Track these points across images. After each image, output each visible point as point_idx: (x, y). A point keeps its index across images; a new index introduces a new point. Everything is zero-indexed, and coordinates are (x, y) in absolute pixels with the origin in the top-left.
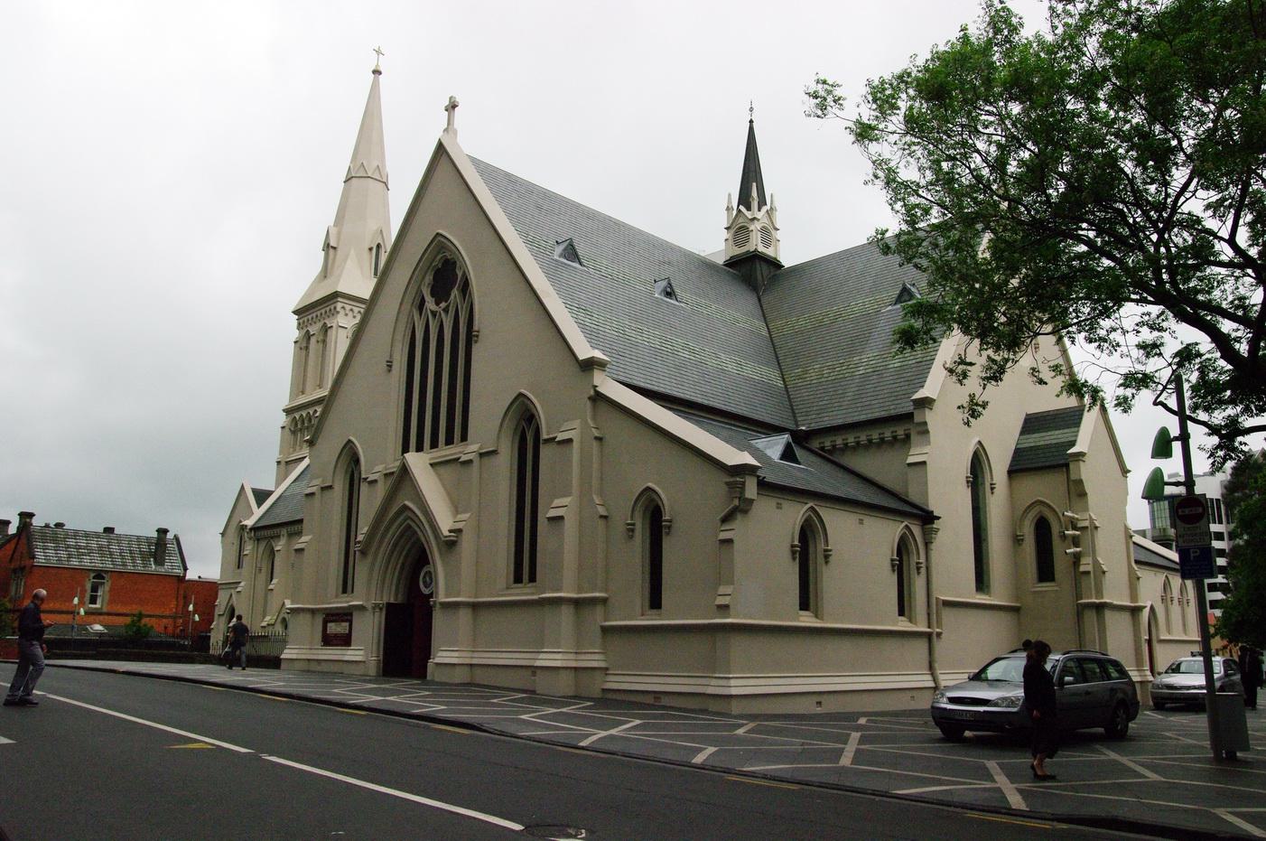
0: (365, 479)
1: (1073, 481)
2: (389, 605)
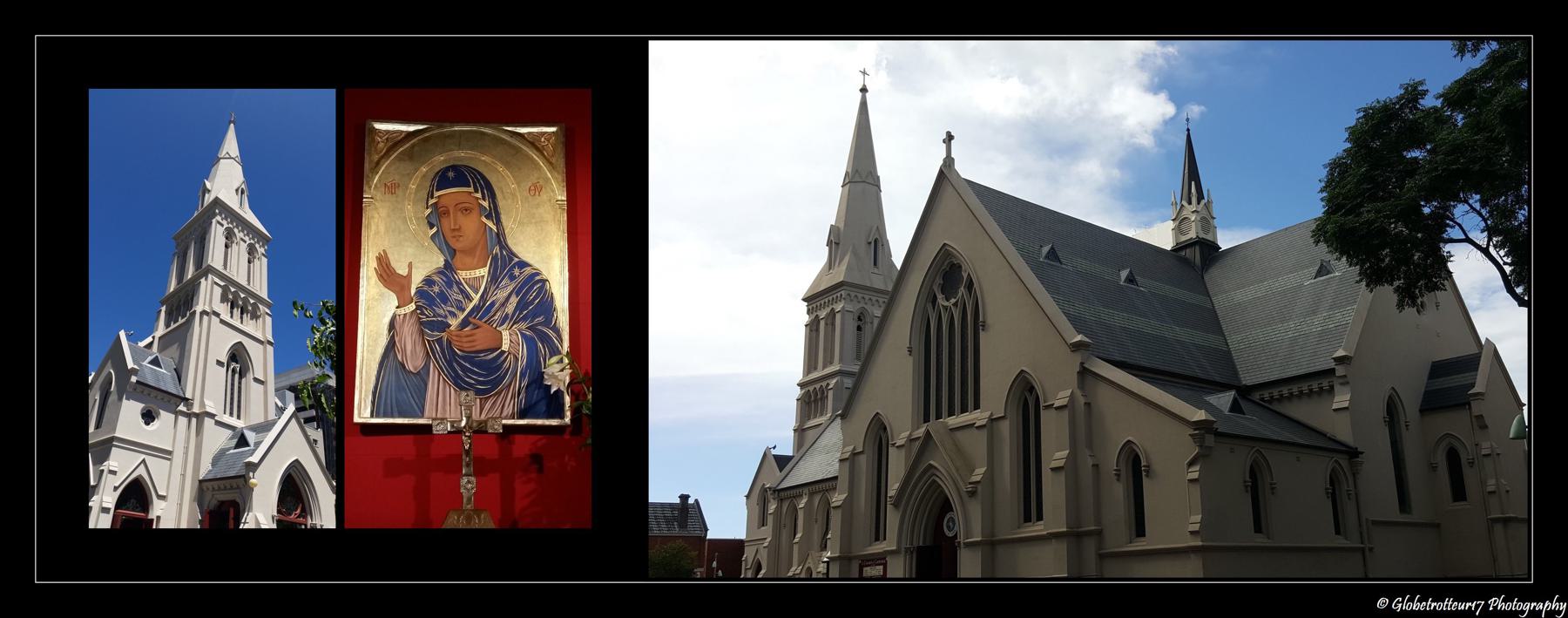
0: (893, 445)
1: (1476, 416)
2: (919, 548)
